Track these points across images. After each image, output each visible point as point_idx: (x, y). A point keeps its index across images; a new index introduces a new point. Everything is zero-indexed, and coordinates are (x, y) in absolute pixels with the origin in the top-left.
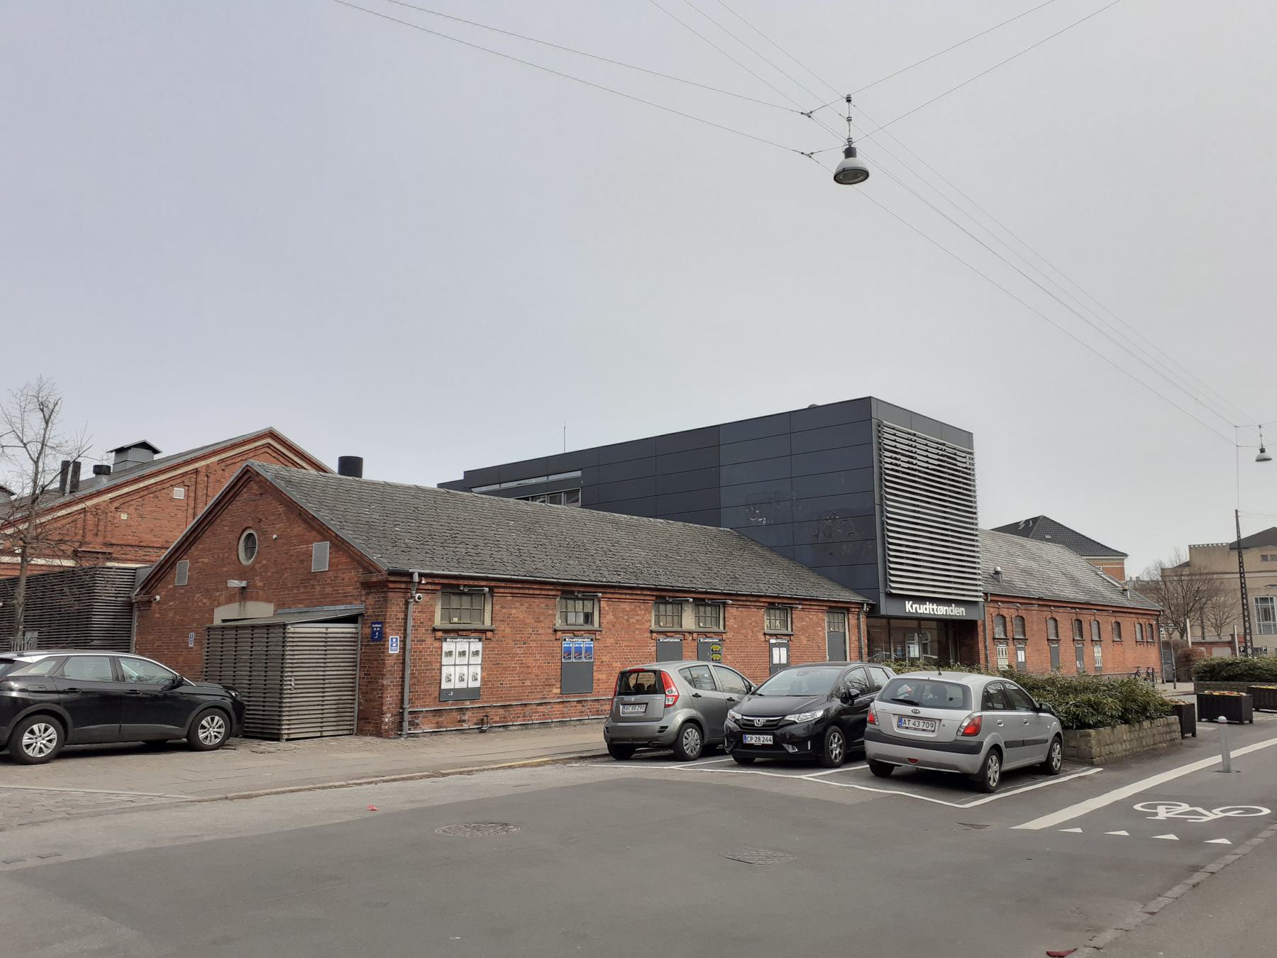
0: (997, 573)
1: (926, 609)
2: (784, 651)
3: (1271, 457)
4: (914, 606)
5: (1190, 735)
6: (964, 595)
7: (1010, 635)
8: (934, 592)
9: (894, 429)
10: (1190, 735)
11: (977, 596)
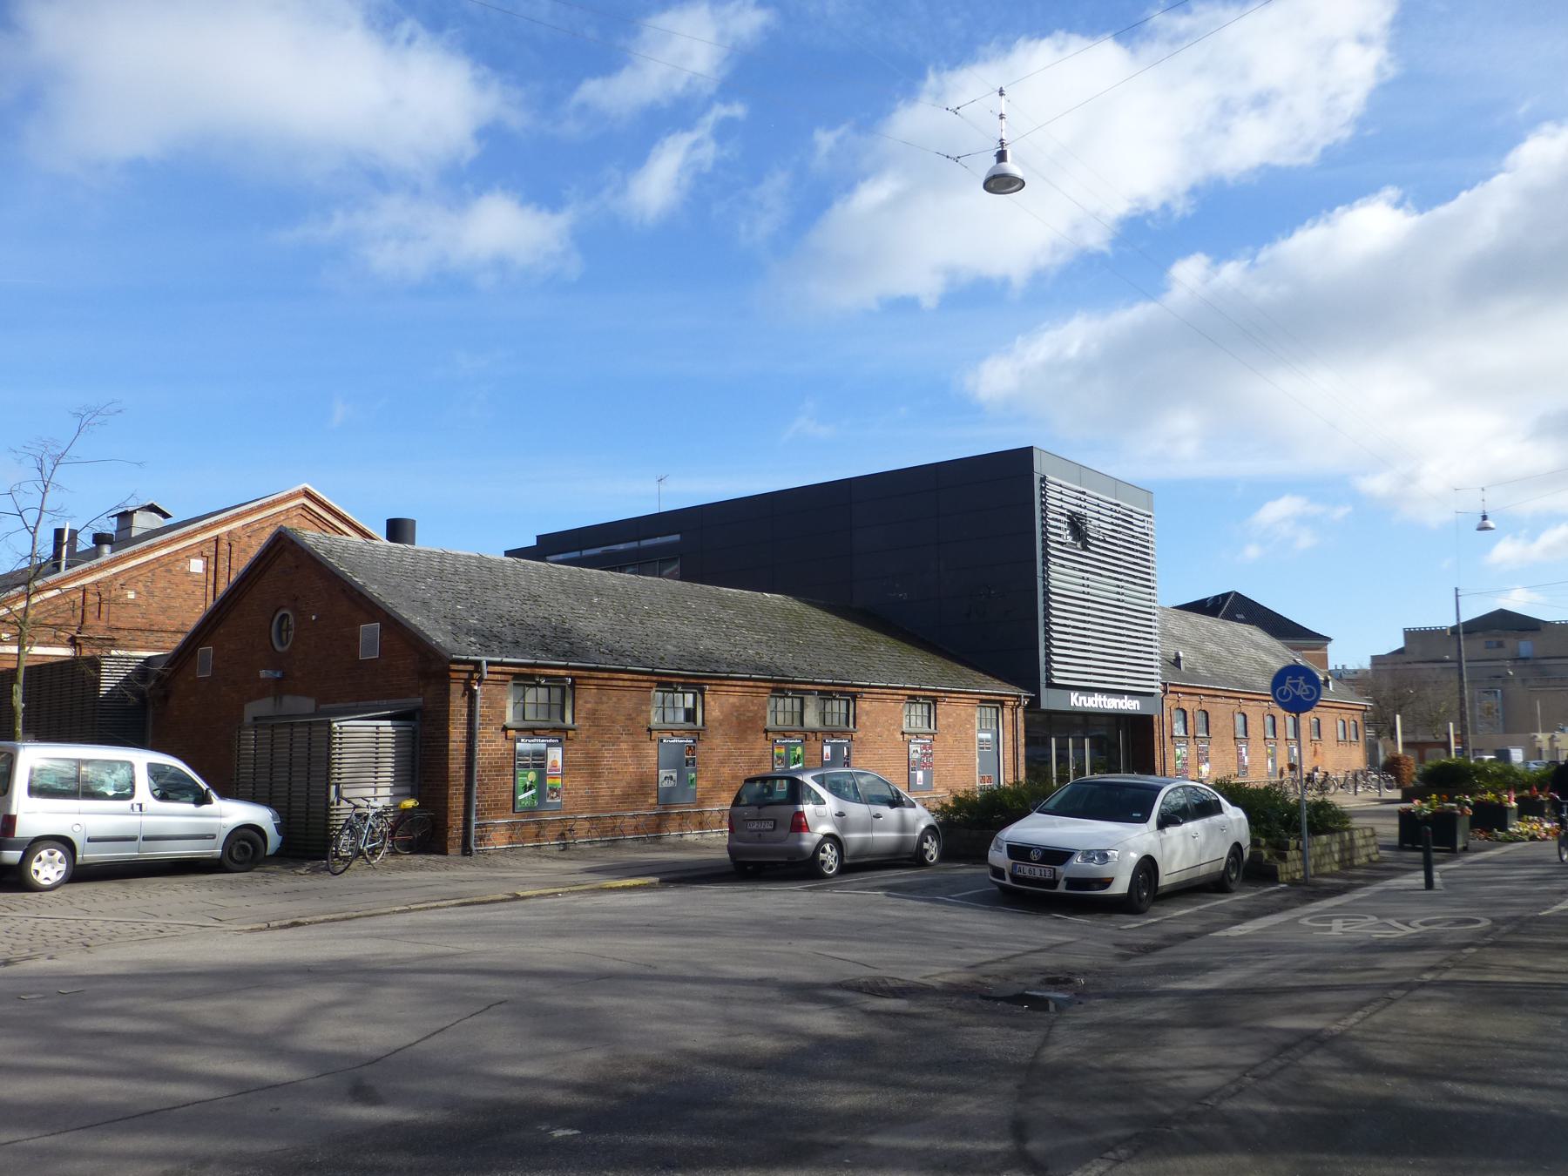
4: (1081, 698)
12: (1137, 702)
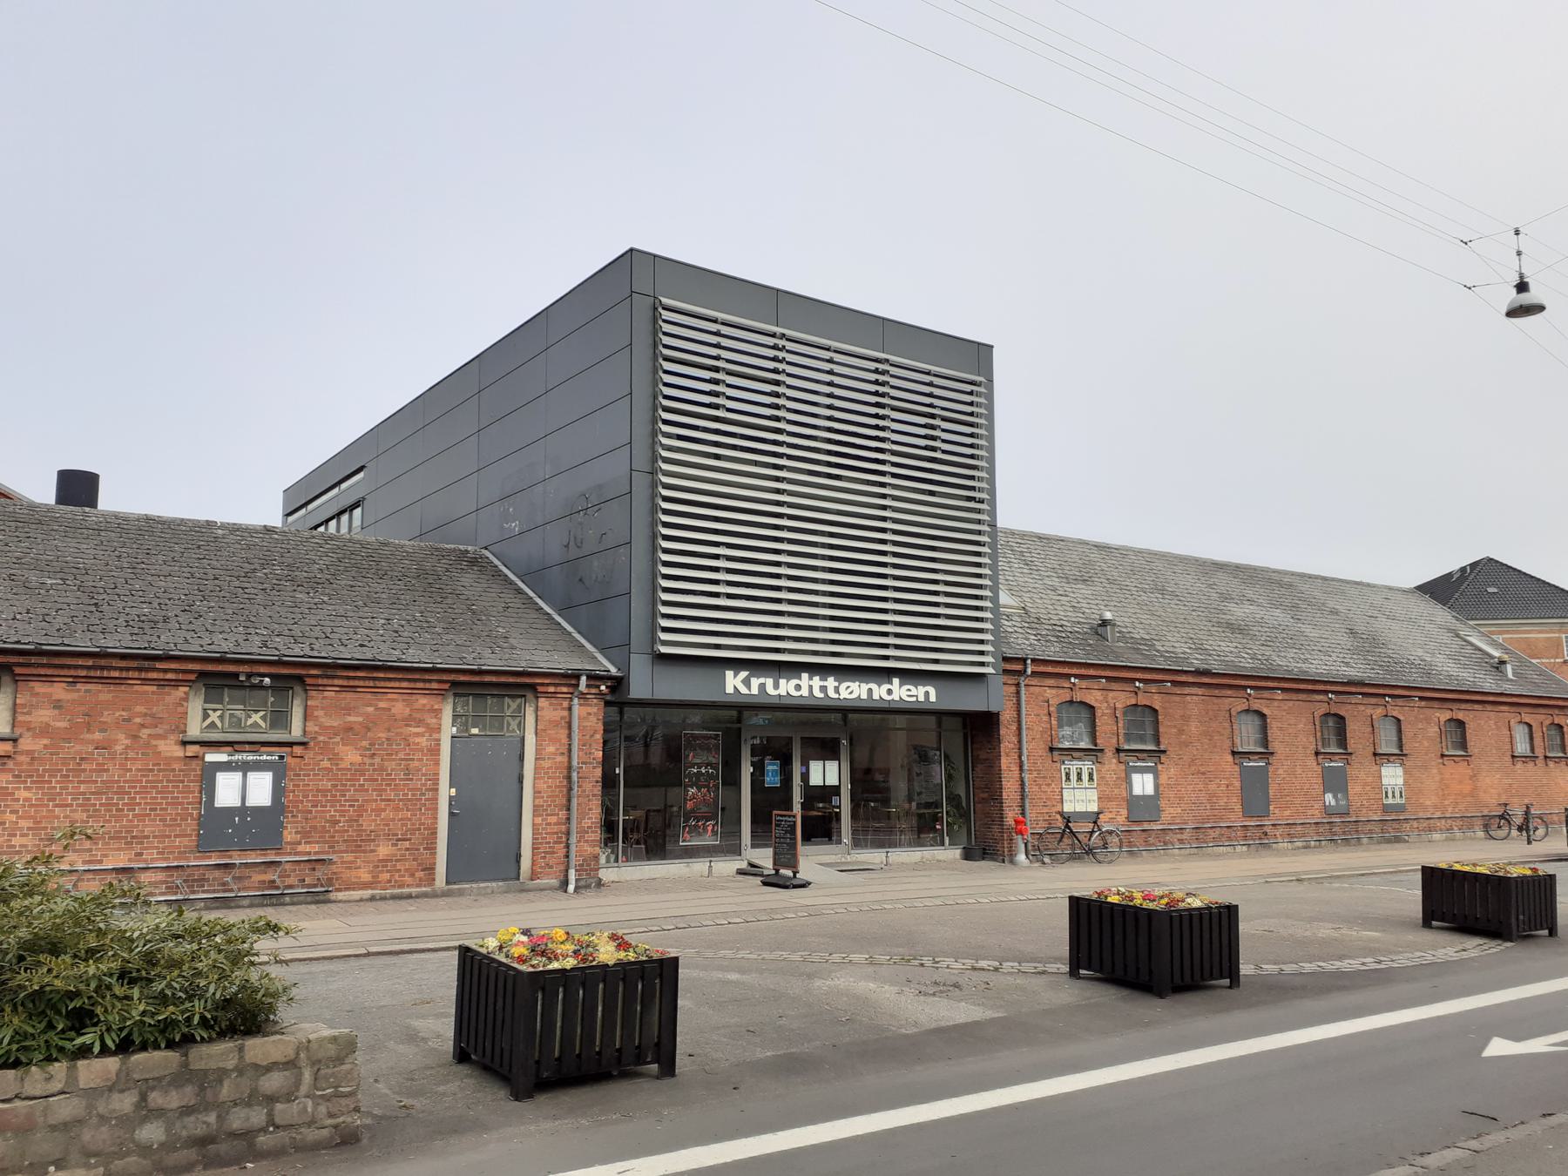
0: (1104, 623)
1: (798, 687)
2: (1149, 778)
3: (1545, 303)
5: (1546, 932)
6: (936, 661)
7: (1539, 752)
8: (717, 647)
9: (928, 373)
10: (1546, 932)
11: (982, 664)
12: (932, 691)
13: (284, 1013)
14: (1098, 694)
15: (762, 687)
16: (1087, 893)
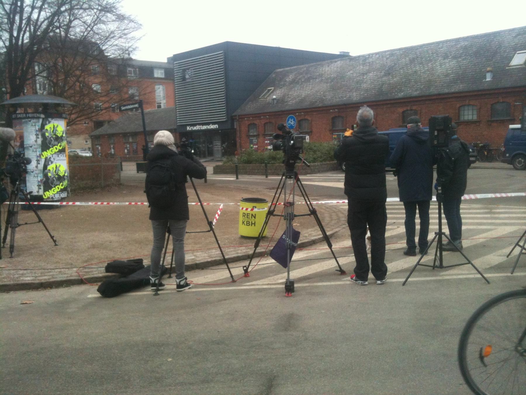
1: (197, 128)
13: (403, 253)
14: (258, 121)
15: (192, 128)
16: (27, 215)
